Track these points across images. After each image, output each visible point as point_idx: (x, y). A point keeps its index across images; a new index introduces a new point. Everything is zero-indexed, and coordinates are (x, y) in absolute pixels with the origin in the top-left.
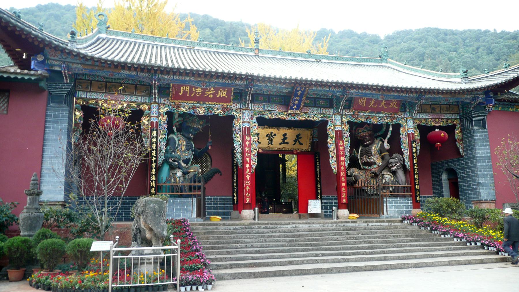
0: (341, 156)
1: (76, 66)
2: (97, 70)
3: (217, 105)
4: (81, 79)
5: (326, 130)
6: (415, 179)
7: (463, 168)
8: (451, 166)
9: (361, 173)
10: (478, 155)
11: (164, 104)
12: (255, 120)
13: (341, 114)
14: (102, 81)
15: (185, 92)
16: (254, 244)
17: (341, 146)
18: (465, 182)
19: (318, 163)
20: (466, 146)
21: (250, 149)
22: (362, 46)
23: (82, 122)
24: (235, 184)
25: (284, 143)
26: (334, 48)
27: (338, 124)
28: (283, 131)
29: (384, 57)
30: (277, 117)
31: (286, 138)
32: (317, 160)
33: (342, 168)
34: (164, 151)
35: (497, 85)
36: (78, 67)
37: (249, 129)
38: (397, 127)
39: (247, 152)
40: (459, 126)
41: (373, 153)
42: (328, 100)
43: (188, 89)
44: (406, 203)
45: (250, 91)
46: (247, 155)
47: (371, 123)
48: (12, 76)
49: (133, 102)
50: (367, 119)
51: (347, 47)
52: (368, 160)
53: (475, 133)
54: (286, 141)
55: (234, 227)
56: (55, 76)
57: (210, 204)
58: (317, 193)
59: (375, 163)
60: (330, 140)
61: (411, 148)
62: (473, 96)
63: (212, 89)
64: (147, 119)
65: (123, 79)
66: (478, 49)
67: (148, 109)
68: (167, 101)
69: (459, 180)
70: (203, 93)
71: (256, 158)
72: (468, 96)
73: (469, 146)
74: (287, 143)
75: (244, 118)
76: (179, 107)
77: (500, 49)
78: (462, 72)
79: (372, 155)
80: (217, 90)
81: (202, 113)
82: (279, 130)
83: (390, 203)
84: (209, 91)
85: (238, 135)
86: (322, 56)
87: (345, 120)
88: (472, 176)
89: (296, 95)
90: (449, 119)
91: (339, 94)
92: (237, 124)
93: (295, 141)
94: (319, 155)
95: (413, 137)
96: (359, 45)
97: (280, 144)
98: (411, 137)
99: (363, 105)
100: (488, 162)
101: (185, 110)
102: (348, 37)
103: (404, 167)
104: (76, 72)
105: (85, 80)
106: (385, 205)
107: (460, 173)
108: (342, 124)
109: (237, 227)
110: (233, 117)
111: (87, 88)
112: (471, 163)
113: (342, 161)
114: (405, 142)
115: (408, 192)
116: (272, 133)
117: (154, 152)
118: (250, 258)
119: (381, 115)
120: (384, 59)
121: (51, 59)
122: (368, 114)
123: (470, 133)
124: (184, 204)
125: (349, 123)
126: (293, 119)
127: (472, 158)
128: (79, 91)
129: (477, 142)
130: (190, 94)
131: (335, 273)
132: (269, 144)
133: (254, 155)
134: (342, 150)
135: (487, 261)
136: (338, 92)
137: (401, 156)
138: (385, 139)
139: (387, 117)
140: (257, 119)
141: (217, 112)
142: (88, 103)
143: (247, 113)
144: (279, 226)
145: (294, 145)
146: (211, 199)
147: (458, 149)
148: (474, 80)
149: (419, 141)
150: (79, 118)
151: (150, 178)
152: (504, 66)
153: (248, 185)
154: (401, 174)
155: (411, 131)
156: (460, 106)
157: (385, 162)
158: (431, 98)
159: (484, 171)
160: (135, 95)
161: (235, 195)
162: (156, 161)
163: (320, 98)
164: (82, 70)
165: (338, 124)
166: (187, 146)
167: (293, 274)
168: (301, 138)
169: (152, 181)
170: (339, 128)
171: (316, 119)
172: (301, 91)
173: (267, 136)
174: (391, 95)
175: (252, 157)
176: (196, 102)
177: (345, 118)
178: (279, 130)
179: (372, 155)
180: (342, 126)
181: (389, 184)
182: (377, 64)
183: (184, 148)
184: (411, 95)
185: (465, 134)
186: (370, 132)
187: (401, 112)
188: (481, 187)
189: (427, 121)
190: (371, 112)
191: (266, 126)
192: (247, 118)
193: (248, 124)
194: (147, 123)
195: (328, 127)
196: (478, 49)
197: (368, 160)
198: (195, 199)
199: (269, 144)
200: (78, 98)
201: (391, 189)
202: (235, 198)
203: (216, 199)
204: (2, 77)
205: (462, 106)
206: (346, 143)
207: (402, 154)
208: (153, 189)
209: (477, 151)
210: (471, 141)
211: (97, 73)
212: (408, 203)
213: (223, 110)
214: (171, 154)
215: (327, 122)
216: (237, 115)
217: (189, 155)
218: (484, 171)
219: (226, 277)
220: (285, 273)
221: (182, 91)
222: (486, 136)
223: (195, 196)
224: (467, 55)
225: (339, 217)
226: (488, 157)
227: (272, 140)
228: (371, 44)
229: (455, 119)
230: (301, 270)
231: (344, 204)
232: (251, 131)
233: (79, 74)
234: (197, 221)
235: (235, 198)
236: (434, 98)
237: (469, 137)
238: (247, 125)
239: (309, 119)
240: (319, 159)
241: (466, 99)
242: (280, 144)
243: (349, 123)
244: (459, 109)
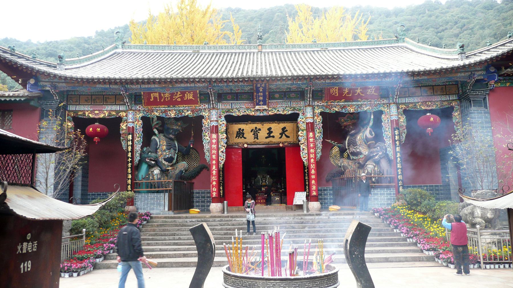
0: (311, 148)
1: (61, 85)
2: (77, 87)
3: (187, 107)
4: (72, 95)
6: (398, 169)
9: (350, 163)
11: (139, 110)
12: (223, 119)
13: (312, 106)
15: (155, 98)
16: (181, 237)
22: (474, 14)
25: (269, 137)
26: (440, 20)
28: (267, 126)
29: (400, 37)
30: (245, 114)
31: (272, 132)
33: (312, 160)
35: (497, 57)
36: (63, 86)
37: (217, 127)
41: (358, 143)
42: (299, 93)
44: (387, 194)
47: (347, 112)
48: (8, 99)
49: (113, 111)
50: (342, 108)
51: (455, 18)
54: (271, 135)
55: (191, 220)
56: (45, 96)
57: (199, 197)
58: (305, 185)
59: (360, 153)
62: (470, 73)
63: (179, 93)
67: (126, 116)
70: (172, 97)
71: (225, 155)
72: (463, 74)
74: (273, 137)
75: (213, 117)
76: (153, 112)
78: (458, 47)
80: (183, 93)
81: (173, 115)
82: (263, 125)
84: (176, 96)
85: (207, 134)
86: (329, 44)
87: (318, 111)
89: (258, 91)
90: (444, 101)
91: (304, 87)
92: (205, 123)
93: (281, 134)
96: (470, 13)
97: (266, 138)
99: (336, 94)
102: (457, 7)
103: (386, 156)
104: (62, 90)
109: (194, 220)
110: (202, 117)
111: (76, 102)
114: (387, 129)
116: (256, 128)
117: (130, 153)
118: (158, 249)
119: (359, 103)
120: (400, 39)
121: (42, 81)
124: (157, 199)
126: (262, 114)
131: (216, 266)
132: (255, 138)
133: (222, 152)
135: (394, 260)
136: (302, 84)
139: (365, 104)
140: (225, 117)
143: (214, 112)
144: (234, 219)
145: (280, 138)
146: (199, 193)
148: (475, 55)
149: (405, 127)
150: (71, 128)
152: (508, 35)
153: (215, 181)
155: (394, 118)
156: (459, 85)
161: (221, 188)
162: (132, 162)
163: (290, 91)
167: (174, 265)
168: (287, 131)
169: (129, 179)
170: (310, 120)
171: (285, 112)
172: (262, 87)
173: (251, 131)
175: (220, 154)
178: (263, 125)
180: (313, 118)
181: (371, 175)
182: (393, 45)
183: (165, 147)
189: (415, 105)
190: (345, 102)
191: (250, 122)
192: (214, 118)
193: (216, 122)
194: (125, 128)
198: (167, 194)
199: (255, 138)
200: (69, 111)
201: (374, 180)
202: (221, 192)
203: (204, 193)
204: (1, 100)
205: (461, 85)
207: (384, 142)
208: (129, 187)
211: (78, 89)
212: (391, 194)
213: (192, 111)
214: (148, 154)
215: (297, 115)
216: (206, 115)
219: (112, 266)
220: (167, 265)
223: (166, 191)
228: (484, 10)
229: (453, 100)
230: (182, 262)
231: (314, 196)
232: (219, 129)
233: (70, 91)
234: (169, 214)
235: (221, 192)
238: (214, 124)
239: (278, 113)
241: (460, 77)
242: (266, 138)
243: (322, 114)
244: (458, 89)
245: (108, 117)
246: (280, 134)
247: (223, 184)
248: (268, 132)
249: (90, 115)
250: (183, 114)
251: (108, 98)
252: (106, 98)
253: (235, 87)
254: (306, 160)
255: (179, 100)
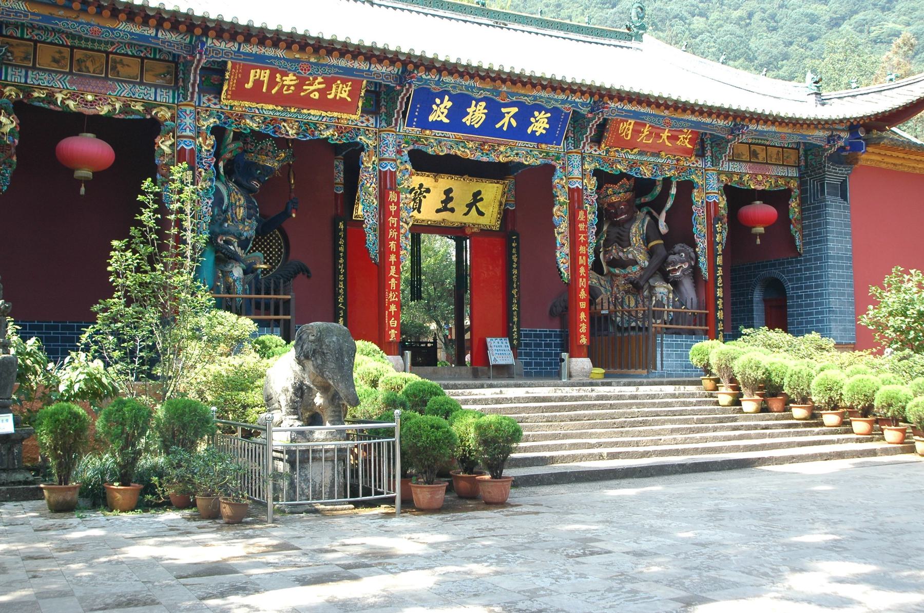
0: (580, 243)
4: (11, 37)
5: (550, 186)
7: (799, 279)
8: (775, 273)
9: (602, 282)
10: (831, 253)
12: (406, 158)
14: (63, 45)
15: (258, 83)
17: (582, 222)
18: (800, 306)
19: (515, 258)
20: (809, 235)
21: (398, 222)
23: (17, 141)
24: (341, 299)
25: (445, 209)
27: (575, 173)
28: (445, 182)
31: (451, 199)
32: (514, 251)
34: (208, 219)
38: (687, 187)
39: (393, 227)
40: (797, 191)
43: (265, 76)
45: (199, 61)
46: (392, 233)
52: (621, 254)
53: (829, 210)
54: (449, 206)
59: (635, 262)
60: (559, 210)
61: (712, 233)
63: (320, 79)
64: (169, 143)
65: (112, 44)
66: (750, 15)
67: (173, 118)
68: (214, 101)
69: (790, 302)
70: (299, 87)
73: (815, 234)
74: (452, 210)
77: (796, 22)
79: (630, 245)
83: (668, 346)
88: (817, 295)
90: (781, 177)
91: (584, 111)
93: (470, 206)
94: (517, 241)
95: (716, 211)
97: (438, 211)
98: (576, 196)
100: (848, 268)
101: (255, 126)
103: (695, 272)
105: (22, 38)
106: (659, 350)
107: (793, 289)
108: (584, 175)
111: (26, 58)
112: (817, 268)
113: (582, 255)
115: (701, 325)
122: (633, 157)
123: (819, 207)
125: (597, 173)
126: (485, 159)
127: (820, 259)
128: (7, 65)
129: (830, 228)
130: (270, 87)
134: (583, 232)
136: (583, 104)
137: (691, 250)
138: (659, 213)
141: (327, 134)
142: (28, 95)
145: (466, 214)
147: (793, 239)
149: (725, 220)
151: (577, 306)
154: (687, 286)
156: (801, 152)
157: (656, 261)
158: (755, 130)
159: (840, 285)
160: (141, 83)
164: (26, 16)
165: (575, 173)
166: (249, 208)
168: (482, 199)
174: (684, 120)
175: (402, 240)
176: (279, 108)
177: (590, 164)
178: (436, 181)
179: (630, 245)
184: (721, 123)
185: (809, 209)
186: (629, 195)
187: (696, 156)
188: (832, 317)
189: (741, 178)
194: (167, 150)
195: (556, 181)
196: (750, 15)
197: (621, 254)
205: (806, 151)
206: (589, 215)
207: (694, 245)
209: (831, 245)
210: (819, 225)
215: (552, 169)
217: (248, 230)
218: (840, 285)
221: (252, 78)
222: (845, 216)
224: (729, 27)
225: (573, 374)
226: (848, 258)
227: (420, 201)
229: (791, 178)
236: (762, 133)
237: (815, 217)
240: (517, 248)
242: (438, 211)
243: (597, 173)
245: (122, 116)
246: (467, 206)
247: (345, 312)
248: (444, 197)
249: (71, 104)
250: (316, 133)
251: (121, 62)
252: (114, 61)
253: (454, 88)
254: (566, 269)
255: (316, 96)
